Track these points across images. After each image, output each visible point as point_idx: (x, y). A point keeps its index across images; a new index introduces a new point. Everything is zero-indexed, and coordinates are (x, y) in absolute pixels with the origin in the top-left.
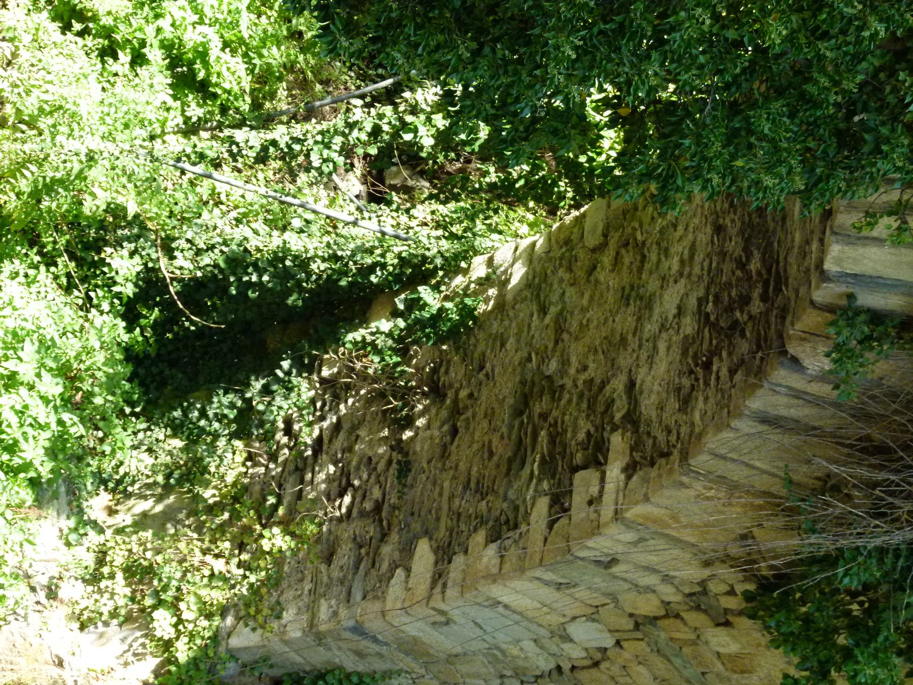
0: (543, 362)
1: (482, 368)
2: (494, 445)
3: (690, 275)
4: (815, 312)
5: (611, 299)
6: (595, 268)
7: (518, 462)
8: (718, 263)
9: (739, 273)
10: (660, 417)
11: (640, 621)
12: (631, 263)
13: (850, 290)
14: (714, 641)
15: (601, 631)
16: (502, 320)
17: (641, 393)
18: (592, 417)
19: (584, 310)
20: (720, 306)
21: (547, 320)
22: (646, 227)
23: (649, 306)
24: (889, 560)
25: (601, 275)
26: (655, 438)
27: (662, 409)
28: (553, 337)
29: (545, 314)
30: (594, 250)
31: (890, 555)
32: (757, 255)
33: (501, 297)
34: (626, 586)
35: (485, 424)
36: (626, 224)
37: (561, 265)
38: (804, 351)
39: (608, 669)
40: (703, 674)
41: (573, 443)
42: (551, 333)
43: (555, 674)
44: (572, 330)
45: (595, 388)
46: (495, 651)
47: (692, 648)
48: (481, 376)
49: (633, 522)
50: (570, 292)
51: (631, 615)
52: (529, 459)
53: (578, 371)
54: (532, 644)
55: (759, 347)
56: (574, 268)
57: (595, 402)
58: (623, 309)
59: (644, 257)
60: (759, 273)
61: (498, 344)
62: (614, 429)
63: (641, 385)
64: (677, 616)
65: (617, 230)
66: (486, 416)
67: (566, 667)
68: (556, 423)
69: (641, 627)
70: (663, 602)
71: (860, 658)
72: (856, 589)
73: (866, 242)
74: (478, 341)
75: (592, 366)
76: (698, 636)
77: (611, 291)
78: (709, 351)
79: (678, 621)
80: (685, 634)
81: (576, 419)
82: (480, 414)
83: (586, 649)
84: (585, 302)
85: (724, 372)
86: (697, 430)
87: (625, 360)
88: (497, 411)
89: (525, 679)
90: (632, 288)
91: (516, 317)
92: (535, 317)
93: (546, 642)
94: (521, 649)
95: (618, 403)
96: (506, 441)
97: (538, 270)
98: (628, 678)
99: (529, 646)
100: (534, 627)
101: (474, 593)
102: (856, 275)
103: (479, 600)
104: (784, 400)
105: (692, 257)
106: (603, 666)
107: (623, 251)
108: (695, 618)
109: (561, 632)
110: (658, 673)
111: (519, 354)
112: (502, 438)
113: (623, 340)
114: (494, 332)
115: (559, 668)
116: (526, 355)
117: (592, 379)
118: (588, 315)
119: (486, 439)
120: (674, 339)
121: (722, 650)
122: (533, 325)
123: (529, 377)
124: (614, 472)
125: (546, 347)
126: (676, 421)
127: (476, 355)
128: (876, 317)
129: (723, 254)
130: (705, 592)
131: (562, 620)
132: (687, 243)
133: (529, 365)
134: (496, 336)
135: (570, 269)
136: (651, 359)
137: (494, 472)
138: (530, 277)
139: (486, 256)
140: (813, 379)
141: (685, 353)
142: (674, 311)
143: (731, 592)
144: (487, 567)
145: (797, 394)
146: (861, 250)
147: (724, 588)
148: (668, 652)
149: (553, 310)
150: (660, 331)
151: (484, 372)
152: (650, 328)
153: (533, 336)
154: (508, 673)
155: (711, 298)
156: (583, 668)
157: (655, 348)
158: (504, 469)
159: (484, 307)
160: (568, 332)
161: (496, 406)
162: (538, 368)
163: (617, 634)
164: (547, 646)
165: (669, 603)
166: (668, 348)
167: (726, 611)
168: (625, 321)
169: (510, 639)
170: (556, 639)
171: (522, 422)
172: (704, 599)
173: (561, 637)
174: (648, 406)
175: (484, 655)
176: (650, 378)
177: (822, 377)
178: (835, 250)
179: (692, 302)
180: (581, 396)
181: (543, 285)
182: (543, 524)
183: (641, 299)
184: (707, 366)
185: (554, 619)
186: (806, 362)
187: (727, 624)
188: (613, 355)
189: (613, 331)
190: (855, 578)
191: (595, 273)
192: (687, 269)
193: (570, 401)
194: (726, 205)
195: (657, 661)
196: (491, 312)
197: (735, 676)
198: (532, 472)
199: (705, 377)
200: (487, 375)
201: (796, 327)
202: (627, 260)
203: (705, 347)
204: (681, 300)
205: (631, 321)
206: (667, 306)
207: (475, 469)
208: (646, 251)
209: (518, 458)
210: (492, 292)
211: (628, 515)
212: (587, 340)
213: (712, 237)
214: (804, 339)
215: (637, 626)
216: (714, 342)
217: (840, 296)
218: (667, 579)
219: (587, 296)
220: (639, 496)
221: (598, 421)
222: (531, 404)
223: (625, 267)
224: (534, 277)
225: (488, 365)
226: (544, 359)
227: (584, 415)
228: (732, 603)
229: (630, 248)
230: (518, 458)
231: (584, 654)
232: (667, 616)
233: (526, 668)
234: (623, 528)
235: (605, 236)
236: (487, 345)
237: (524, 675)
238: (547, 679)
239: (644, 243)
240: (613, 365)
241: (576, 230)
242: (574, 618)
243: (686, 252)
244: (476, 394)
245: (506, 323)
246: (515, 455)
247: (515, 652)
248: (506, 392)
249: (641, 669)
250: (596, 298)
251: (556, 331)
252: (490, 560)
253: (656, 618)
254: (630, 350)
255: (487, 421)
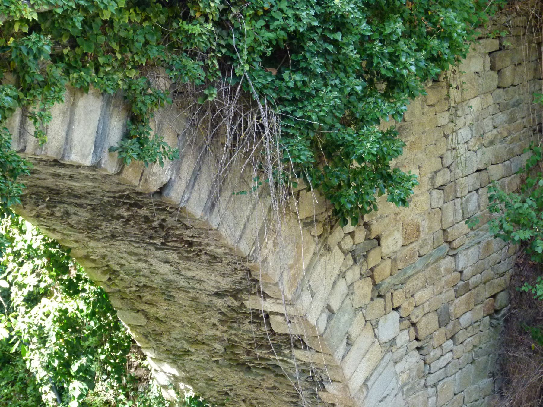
0: (216, 352)
1: (227, 394)
2: (269, 386)
3: (145, 256)
4: (125, 172)
5: (173, 308)
6: (157, 318)
7: (276, 370)
8: (132, 237)
9: (132, 223)
10: (229, 275)
11: (377, 294)
12: (150, 294)
13: (107, 150)
14: (392, 248)
15: (386, 319)
16: (197, 380)
17: (218, 288)
18: (241, 320)
19: (183, 326)
20: (154, 236)
21: (192, 349)
22: (127, 284)
23: (169, 282)
24: (291, 131)
25: (161, 314)
26: (241, 279)
27: (224, 274)
28: (201, 346)
29: (189, 351)
30: (148, 319)
31: (289, 131)
32: (117, 212)
33: (184, 380)
34: (348, 301)
35: (258, 391)
36: (128, 298)
37: (160, 341)
38: (156, 181)
39: (417, 317)
40: (420, 256)
41: (257, 333)
42: (199, 347)
43: (422, 352)
44: (195, 333)
45: (224, 318)
46: (405, 389)
47: (398, 262)
48: (231, 394)
49: (295, 294)
50: (175, 334)
51: (372, 299)
52: (274, 362)
53: (217, 330)
54: (398, 365)
55: (164, 210)
56: (160, 332)
57: (232, 318)
58: (176, 300)
59: (145, 286)
60: (128, 210)
61: (211, 382)
62: (242, 305)
63: (214, 287)
64: (372, 270)
65: (134, 304)
66: (253, 391)
67: (416, 344)
68: (250, 344)
69: (382, 293)
70: (360, 279)
71: (361, 151)
72: (31, 119)
73: (69, 139)
74: (212, 396)
75: (212, 320)
76: (389, 258)
77: (169, 307)
78: (181, 243)
79: (376, 269)
80: (387, 266)
81: (244, 331)
82: (252, 395)
83: (401, 330)
84: (178, 325)
85: (188, 232)
86: (228, 251)
87: (205, 299)
88: (249, 383)
89: (427, 372)
90: (163, 293)
91: (194, 370)
92: (192, 358)
93: (396, 356)
94: (402, 372)
95: (229, 303)
96: (265, 377)
97: (165, 356)
98: (425, 305)
99: (399, 367)
100: (384, 363)
101: (356, 399)
102: (95, 147)
103: (362, 397)
104: (195, 194)
105: (136, 254)
106: (414, 320)
107: (144, 299)
108: (374, 258)
109: (388, 345)
110: (420, 285)
111: (215, 369)
112: (263, 380)
113: (194, 299)
114: (205, 385)
115: (418, 349)
116: (215, 364)
117: (220, 320)
118: (185, 323)
119: (267, 391)
120: (183, 266)
121: (400, 243)
122: (197, 359)
123: (228, 362)
124: (267, 306)
125: (208, 351)
126: (228, 265)
127: (220, 397)
128: (127, 135)
129: (126, 234)
130: (352, 252)
131: (377, 344)
132: (129, 257)
133: (220, 362)
134: (207, 384)
135: (161, 334)
136: (200, 281)
137: (284, 386)
138: (170, 361)
139: (163, 390)
140: (178, 175)
141: (188, 259)
142: (168, 266)
143: (352, 234)
144: (339, 391)
145: (191, 186)
146: (75, 142)
147: (348, 239)
148: (402, 278)
149: (186, 346)
150: (181, 275)
151: (229, 392)
152: (182, 283)
153: (203, 359)
154: (423, 382)
155: (152, 241)
156: (416, 332)
157: (192, 278)
158: (282, 379)
159: (191, 392)
160: (196, 336)
161: (246, 384)
162: (221, 356)
163: (388, 310)
164: (399, 355)
165: (362, 275)
166: (189, 269)
167: (367, 238)
168: (182, 298)
169: (394, 379)
170: (393, 349)
171: (254, 366)
172: (357, 253)
173: (391, 346)
174: (226, 284)
175: (408, 396)
176: (209, 282)
177: (178, 169)
178: (74, 158)
179: (159, 253)
180: (231, 328)
181: (173, 352)
182: (308, 353)
183: (167, 287)
184: (191, 244)
185: (377, 349)
186: (165, 180)
187: (378, 239)
188: (203, 306)
189: (190, 306)
190: (302, 153)
191: (160, 318)
192: (142, 257)
193: (236, 335)
194: (99, 231)
195: (409, 285)
196: (193, 386)
197: (422, 236)
198: (281, 360)
199: (196, 246)
200: (231, 390)
201: (137, 184)
202: (149, 297)
203: (179, 245)
204: (161, 261)
205: (182, 294)
206: (167, 271)
207: (284, 398)
208: (141, 284)
209: (272, 369)
210: (182, 386)
211: (289, 297)
212: (199, 323)
213: (118, 240)
214: (146, 180)
215: (380, 296)
216: (174, 239)
217: (111, 156)
218: (342, 275)
219: (174, 323)
220: (275, 289)
221: (242, 316)
222: (242, 361)
223: (153, 298)
224: (169, 358)
225: (225, 389)
226: (214, 352)
227: (241, 326)
228: (361, 235)
229: (141, 295)
230: (272, 369)
231: (406, 332)
232: (372, 277)
233: (418, 370)
234: (299, 301)
235: (138, 311)
236: (213, 390)
237: (424, 372)
238: (427, 357)
239: (137, 286)
240: (209, 306)
241: (138, 330)
242: (375, 336)
243: (133, 258)
244: (243, 398)
245: (198, 377)
246: (273, 372)
247: (405, 376)
248: (237, 377)
249: (417, 296)
250: (175, 317)
251: (197, 344)
252: (335, 389)
253: (375, 284)
254: (197, 295)
255: (256, 390)
